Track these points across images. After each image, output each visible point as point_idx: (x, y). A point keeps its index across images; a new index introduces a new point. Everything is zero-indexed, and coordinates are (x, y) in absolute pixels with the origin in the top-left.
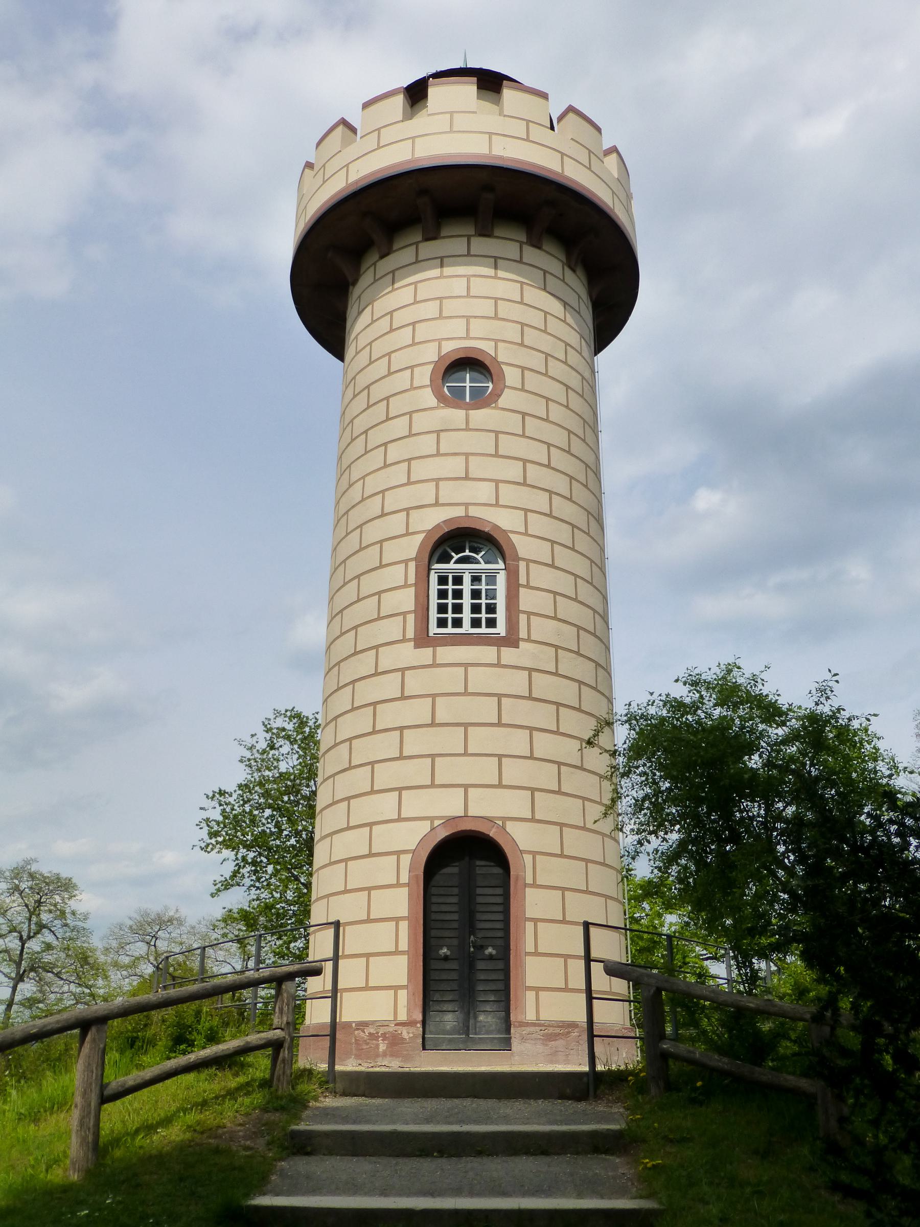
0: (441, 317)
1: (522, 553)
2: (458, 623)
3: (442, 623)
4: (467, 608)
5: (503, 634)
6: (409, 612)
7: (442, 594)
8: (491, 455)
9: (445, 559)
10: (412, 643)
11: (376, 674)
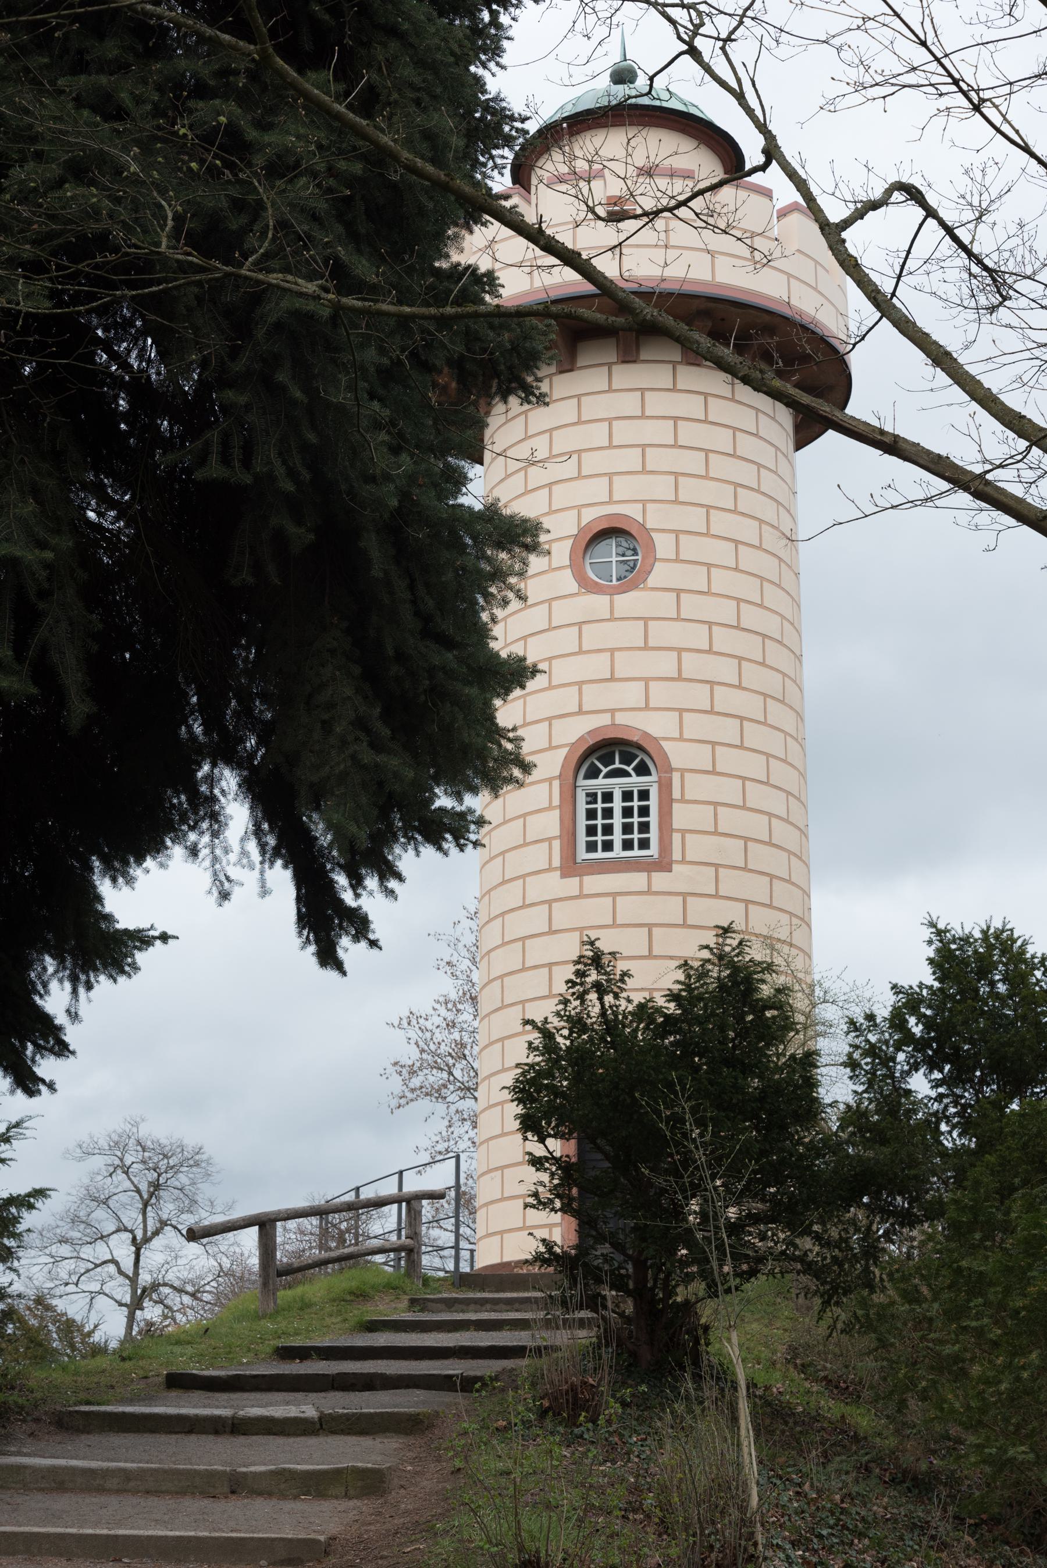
0: (580, 477)
1: (675, 762)
2: (608, 846)
3: (591, 847)
4: (618, 829)
5: (656, 856)
6: (554, 838)
7: (591, 814)
8: (639, 649)
9: (593, 774)
10: (558, 873)
11: (524, 906)
